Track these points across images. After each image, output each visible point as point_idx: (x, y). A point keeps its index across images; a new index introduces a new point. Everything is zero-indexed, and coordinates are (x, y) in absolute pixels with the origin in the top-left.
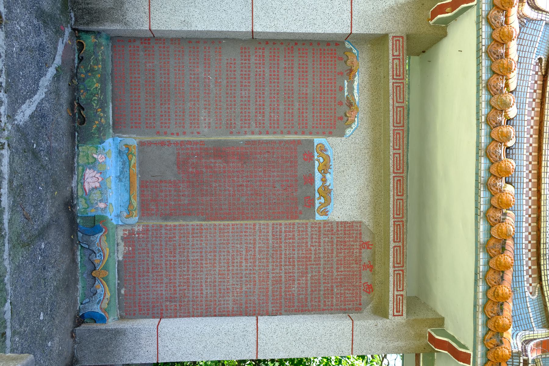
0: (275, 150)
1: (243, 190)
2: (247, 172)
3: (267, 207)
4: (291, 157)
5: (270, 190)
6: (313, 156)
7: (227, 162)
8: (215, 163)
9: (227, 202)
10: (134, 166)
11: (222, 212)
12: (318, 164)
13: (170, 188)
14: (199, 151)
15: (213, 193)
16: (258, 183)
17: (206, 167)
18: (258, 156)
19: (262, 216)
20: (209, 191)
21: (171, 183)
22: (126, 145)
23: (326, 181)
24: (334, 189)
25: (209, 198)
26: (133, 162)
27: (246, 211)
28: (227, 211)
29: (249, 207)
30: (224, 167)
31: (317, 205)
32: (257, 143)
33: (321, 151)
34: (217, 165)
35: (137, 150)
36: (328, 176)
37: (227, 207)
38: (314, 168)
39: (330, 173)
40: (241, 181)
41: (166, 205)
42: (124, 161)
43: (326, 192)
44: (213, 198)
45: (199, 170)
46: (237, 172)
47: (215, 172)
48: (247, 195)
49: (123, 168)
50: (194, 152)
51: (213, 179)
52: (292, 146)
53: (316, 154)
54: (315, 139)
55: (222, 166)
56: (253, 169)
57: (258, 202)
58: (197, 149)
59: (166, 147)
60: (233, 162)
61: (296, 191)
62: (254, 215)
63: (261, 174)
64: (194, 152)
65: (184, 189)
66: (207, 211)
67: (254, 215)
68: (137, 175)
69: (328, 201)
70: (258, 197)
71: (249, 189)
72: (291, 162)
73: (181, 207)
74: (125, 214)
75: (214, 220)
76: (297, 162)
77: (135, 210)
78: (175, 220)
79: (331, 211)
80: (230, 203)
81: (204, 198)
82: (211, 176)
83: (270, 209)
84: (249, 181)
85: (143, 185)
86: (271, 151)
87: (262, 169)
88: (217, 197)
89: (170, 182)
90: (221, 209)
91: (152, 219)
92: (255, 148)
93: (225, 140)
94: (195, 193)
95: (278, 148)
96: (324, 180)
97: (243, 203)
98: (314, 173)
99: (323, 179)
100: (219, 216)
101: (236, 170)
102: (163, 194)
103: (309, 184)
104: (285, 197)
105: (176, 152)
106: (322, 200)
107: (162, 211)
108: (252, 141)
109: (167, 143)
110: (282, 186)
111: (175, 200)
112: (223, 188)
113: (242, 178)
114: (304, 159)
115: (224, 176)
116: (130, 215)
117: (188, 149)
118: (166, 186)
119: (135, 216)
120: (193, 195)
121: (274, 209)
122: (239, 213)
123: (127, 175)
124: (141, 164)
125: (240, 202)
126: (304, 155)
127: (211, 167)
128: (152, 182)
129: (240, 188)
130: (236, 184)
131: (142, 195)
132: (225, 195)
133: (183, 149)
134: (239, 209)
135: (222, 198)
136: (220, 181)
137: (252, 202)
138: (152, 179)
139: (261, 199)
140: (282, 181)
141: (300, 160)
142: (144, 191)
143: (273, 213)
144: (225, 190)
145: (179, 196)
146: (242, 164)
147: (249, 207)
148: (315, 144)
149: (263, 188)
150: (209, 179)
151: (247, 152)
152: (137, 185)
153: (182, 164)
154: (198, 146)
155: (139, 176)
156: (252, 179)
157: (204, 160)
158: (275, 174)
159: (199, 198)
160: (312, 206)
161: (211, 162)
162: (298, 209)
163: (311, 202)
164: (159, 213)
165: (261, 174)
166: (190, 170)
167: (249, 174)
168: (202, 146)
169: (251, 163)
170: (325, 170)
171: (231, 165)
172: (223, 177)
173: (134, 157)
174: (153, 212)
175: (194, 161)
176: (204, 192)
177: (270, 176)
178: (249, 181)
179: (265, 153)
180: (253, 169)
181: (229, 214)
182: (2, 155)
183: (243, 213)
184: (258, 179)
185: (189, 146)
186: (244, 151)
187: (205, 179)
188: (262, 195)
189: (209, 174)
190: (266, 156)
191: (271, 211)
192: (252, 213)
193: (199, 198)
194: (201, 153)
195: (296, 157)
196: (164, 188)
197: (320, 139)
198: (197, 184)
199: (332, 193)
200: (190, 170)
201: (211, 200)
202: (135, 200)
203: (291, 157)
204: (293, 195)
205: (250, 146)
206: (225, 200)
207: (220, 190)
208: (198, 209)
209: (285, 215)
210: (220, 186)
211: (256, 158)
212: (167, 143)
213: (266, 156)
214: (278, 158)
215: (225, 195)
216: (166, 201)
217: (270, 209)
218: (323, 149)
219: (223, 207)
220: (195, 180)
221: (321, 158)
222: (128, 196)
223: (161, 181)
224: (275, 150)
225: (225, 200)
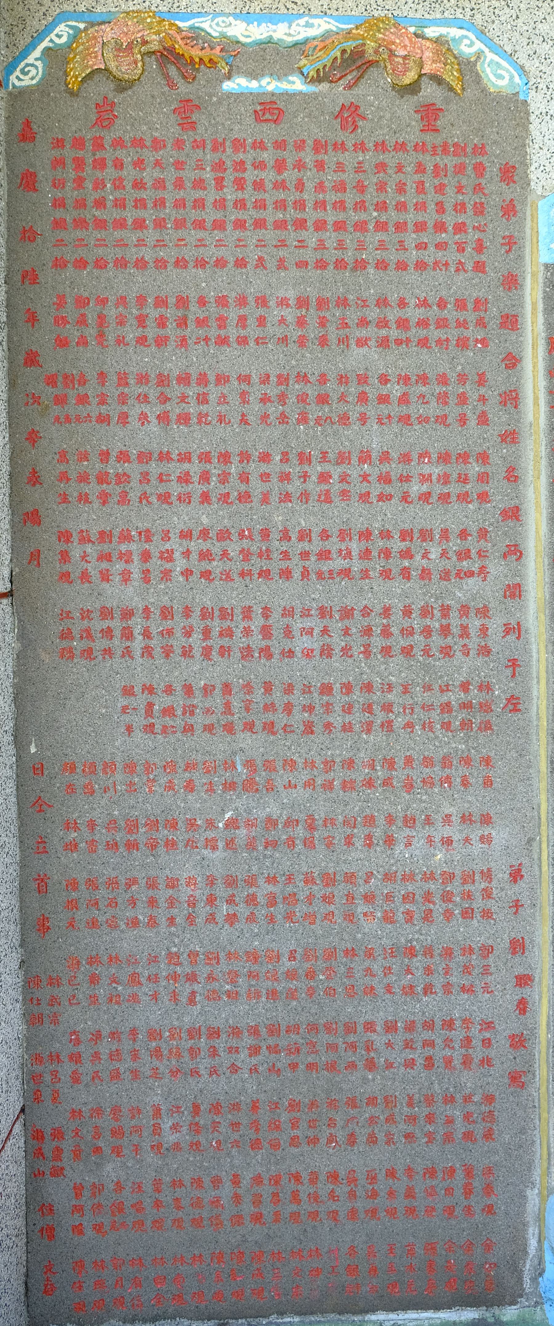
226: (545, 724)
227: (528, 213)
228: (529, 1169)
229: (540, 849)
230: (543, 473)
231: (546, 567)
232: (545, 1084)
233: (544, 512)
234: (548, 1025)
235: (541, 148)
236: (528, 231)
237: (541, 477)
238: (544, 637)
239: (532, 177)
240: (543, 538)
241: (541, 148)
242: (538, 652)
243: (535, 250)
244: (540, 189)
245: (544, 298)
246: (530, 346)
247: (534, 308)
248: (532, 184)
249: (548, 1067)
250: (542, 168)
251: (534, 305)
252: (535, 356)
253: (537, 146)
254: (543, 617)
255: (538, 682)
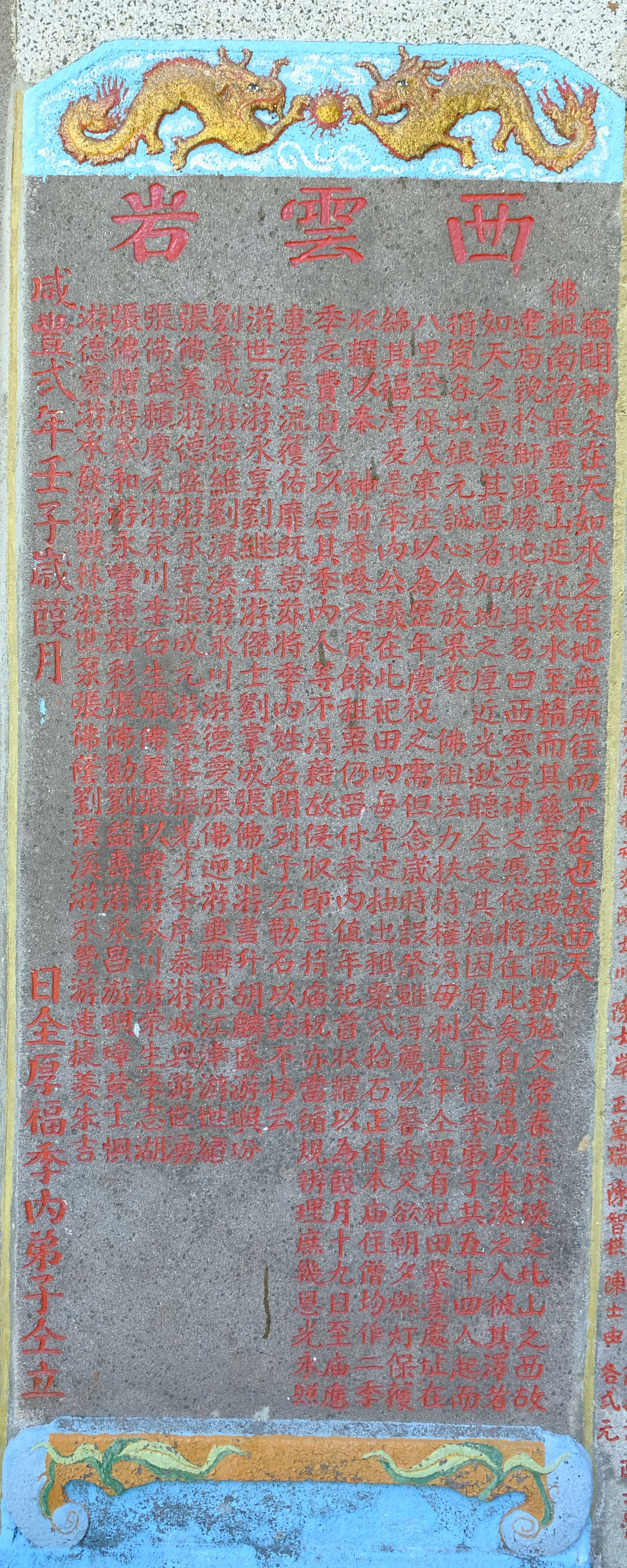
0: (106, 467)
1: (382, 710)
2: (254, 670)
3: (515, 537)
4: (157, 349)
5: (394, 509)
6: (155, 183)
7: (185, 811)
8: (183, 895)
9: (468, 827)
10: (195, 1453)
11: (534, 862)
12: (214, 150)
13: (355, 1215)
14: (101, 1010)
15: (397, 917)
16: (340, 597)
17: (214, 960)
18: (144, 590)
19: (574, 576)
20: (381, 948)
21: (315, 1205)
22: (51, 1496)
23: (337, 98)
24: (399, 34)
25: (433, 952)
26: (162, 1458)
27: (537, 693)
28: (532, 822)
29: (510, 664)
30: (219, 837)
31: (514, 167)
32: (49, 594)
33: (112, 125)
34: (198, 884)
35: (83, 1428)
36: (300, 80)
37: (499, 828)
38: (238, 180)
39: (282, 63)
40: (317, 723)
41: (470, 1244)
42: (157, 1514)
43: (419, 95)
44: (433, 919)
45: (231, 1009)
46: (251, 745)
47: (249, 902)
48: (421, 678)
49: (207, 1522)
50: (105, 1039)
51: (302, 916)
52: (72, 343)
53: (138, 166)
54: (29, 167)
55: (207, 852)
56: (236, 633)
57: (473, 602)
58: (85, 1020)
59: (66, 1229)
60: (184, 771)
61: (400, 320)
62: (570, 636)
63: (270, 576)
64: (105, 1039)
65: (363, 1119)
66: (526, 964)
67: (570, 636)
68: (258, 1429)
69: (490, 86)
70: (441, 598)
71: (376, 666)
72: (192, 349)
73: (491, 1140)
74: (521, 1521)
75: (592, 917)
76: (195, 310)
77: (500, 1458)
78: (575, 1186)
79: (563, 66)
80: (474, 801)
81: (430, 984)
82: (281, 930)
83: (527, 518)
84: (323, 665)
85: (325, 1392)
86: (109, 494)
87: (238, 567)
88: (429, 890)
89: (309, 1210)
90: (514, 864)
91: (565, 1339)
92: (82, 615)
93: (26, 823)
94: (393, 1043)
95: (90, 447)
96: (333, 110)
97: (481, 713)
98: (276, 184)
99: (324, 114)
100: (563, 886)
101: (237, 755)
102: (393, 1262)
103: (356, 225)
104: (446, 406)
105: (100, 1166)
106: (480, 126)
107: (513, 1270)
108: (36, 630)
109: (43, 1223)
110: (363, 422)
111: (440, 1184)
112: (369, 851)
113: (296, 710)
114: (170, 256)
115: (281, 836)
116: (535, 1494)
117: (83, 1085)
118: (341, 1238)
119: (538, 1455)
120: (411, 1059)
121: (531, 487)
122: (548, 740)
123: (251, 1498)
124: (176, 1399)
125: (469, 729)
126: (140, 255)
127: (216, 929)
128: (305, 1335)
129: (371, 726)
130: (338, 758)
131: (394, 1402)
132: (417, 833)
133: (85, 1119)
134: (517, 741)
135: (435, 855)
136: (317, 868)
137: (471, 642)
138: (287, 1328)
139: (456, 582)
140: (328, 420)
141: (184, 284)
142: (367, 1389)
143: (558, 490)
144: (383, 835)
145: (408, 1155)
146: (202, 708)
147: (510, 664)
148: (66, 167)
149: (373, 565)
150: (298, 946)
151: (115, 671)
152: (320, 1434)
153: (184, 1129)
154: (64, 1011)
155: (264, 1414)
156: (308, 642)
157: (167, 978)
158: (275, 470)
159: (428, 1021)
160: (522, 209)
161: (181, 925)
162: (534, 314)
163: (494, 219)
164: (521, 1293)
165: (270, 576)
166: (229, 1070)
167: (273, 662)
168: (65, 983)
169: (190, 640)
170: (268, 106)
171: (201, 785)
172: (284, 848)
173: (130, 1450)
174: (515, 1329)
175: (167, 1041)
176: (391, 981)
177: (292, 511)
178: (323, 665)
179: (123, 544)
180: (236, 633)
181: (550, 812)
182: (623, 853)
183: (551, 713)
184: (307, 596)
185: (65, 1076)
186: (103, 692)
187: (296, 972)
188: (423, 571)
189: (263, 943)
190: (142, 532)
191: (547, 512)
192: (554, 647)
193: (428, 1021)
194: (111, 995)
195: (154, 315)
196: (353, 1256)
197: (28, 130)
198: (329, 1026)
199: (429, 52)
200: (229, 1070)
201: (450, 938)
202: (425, 1453)
203: (157, 349)
204: (432, 346)
205: (67, 648)
206: (450, 836)
207: (382, 869)
208: (508, 1029)
209: (577, 408)
210: (350, 868)
211: (157, 605)
212: (43, 1223)
213: (142, 532)
214: (157, 446)
215: (417, 833)
216: (441, 1244)
217: (527, 518)
218: (105, 111)
219: (501, 853)
220: (299, 1044)
221: (166, 129)
222: (394, 1492)
223: (306, 1271)
224: (106, 467)
225: (450, 836)
226: (16, 805)
227: (11, 107)
228: (28, 239)
229: (6, 974)
230: (20, 463)
231: (21, 593)
232: (7, 1290)
233: (20, 517)
234: (12, 1210)
235: (31, 18)
236: (10, 131)
237: (17, 469)
238: (16, 688)
239: (18, 57)
240: (17, 553)
241: (31, 18)
242: (8, 709)
243: (17, 158)
244: (28, 73)
245: (27, 224)
246: (8, 289)
247: (14, 238)
248: (19, 67)
249: (12, 1268)
250: (32, 45)
251: (14, 232)
252: (13, 304)
253: (26, 15)
254: (15, 660)
255: (7, 749)
